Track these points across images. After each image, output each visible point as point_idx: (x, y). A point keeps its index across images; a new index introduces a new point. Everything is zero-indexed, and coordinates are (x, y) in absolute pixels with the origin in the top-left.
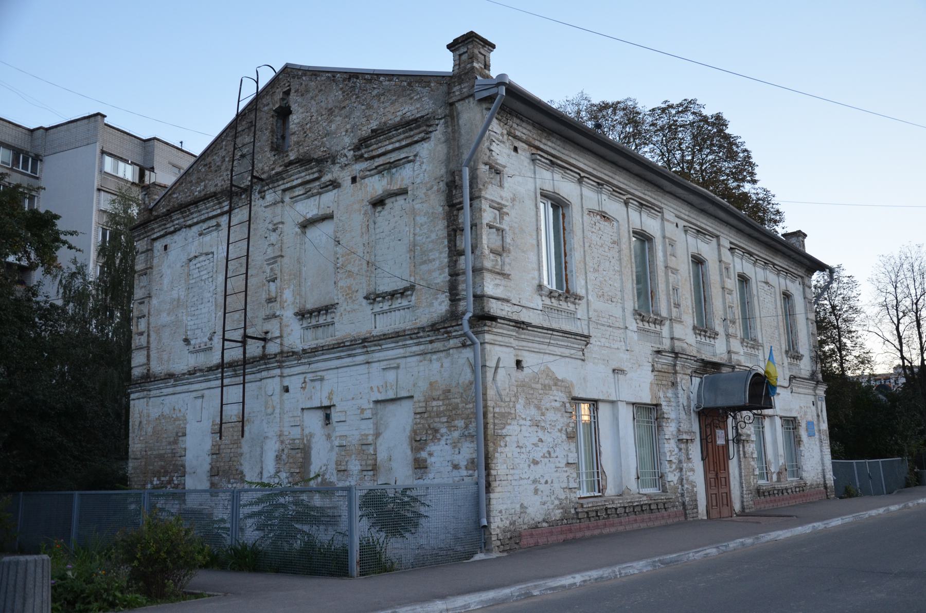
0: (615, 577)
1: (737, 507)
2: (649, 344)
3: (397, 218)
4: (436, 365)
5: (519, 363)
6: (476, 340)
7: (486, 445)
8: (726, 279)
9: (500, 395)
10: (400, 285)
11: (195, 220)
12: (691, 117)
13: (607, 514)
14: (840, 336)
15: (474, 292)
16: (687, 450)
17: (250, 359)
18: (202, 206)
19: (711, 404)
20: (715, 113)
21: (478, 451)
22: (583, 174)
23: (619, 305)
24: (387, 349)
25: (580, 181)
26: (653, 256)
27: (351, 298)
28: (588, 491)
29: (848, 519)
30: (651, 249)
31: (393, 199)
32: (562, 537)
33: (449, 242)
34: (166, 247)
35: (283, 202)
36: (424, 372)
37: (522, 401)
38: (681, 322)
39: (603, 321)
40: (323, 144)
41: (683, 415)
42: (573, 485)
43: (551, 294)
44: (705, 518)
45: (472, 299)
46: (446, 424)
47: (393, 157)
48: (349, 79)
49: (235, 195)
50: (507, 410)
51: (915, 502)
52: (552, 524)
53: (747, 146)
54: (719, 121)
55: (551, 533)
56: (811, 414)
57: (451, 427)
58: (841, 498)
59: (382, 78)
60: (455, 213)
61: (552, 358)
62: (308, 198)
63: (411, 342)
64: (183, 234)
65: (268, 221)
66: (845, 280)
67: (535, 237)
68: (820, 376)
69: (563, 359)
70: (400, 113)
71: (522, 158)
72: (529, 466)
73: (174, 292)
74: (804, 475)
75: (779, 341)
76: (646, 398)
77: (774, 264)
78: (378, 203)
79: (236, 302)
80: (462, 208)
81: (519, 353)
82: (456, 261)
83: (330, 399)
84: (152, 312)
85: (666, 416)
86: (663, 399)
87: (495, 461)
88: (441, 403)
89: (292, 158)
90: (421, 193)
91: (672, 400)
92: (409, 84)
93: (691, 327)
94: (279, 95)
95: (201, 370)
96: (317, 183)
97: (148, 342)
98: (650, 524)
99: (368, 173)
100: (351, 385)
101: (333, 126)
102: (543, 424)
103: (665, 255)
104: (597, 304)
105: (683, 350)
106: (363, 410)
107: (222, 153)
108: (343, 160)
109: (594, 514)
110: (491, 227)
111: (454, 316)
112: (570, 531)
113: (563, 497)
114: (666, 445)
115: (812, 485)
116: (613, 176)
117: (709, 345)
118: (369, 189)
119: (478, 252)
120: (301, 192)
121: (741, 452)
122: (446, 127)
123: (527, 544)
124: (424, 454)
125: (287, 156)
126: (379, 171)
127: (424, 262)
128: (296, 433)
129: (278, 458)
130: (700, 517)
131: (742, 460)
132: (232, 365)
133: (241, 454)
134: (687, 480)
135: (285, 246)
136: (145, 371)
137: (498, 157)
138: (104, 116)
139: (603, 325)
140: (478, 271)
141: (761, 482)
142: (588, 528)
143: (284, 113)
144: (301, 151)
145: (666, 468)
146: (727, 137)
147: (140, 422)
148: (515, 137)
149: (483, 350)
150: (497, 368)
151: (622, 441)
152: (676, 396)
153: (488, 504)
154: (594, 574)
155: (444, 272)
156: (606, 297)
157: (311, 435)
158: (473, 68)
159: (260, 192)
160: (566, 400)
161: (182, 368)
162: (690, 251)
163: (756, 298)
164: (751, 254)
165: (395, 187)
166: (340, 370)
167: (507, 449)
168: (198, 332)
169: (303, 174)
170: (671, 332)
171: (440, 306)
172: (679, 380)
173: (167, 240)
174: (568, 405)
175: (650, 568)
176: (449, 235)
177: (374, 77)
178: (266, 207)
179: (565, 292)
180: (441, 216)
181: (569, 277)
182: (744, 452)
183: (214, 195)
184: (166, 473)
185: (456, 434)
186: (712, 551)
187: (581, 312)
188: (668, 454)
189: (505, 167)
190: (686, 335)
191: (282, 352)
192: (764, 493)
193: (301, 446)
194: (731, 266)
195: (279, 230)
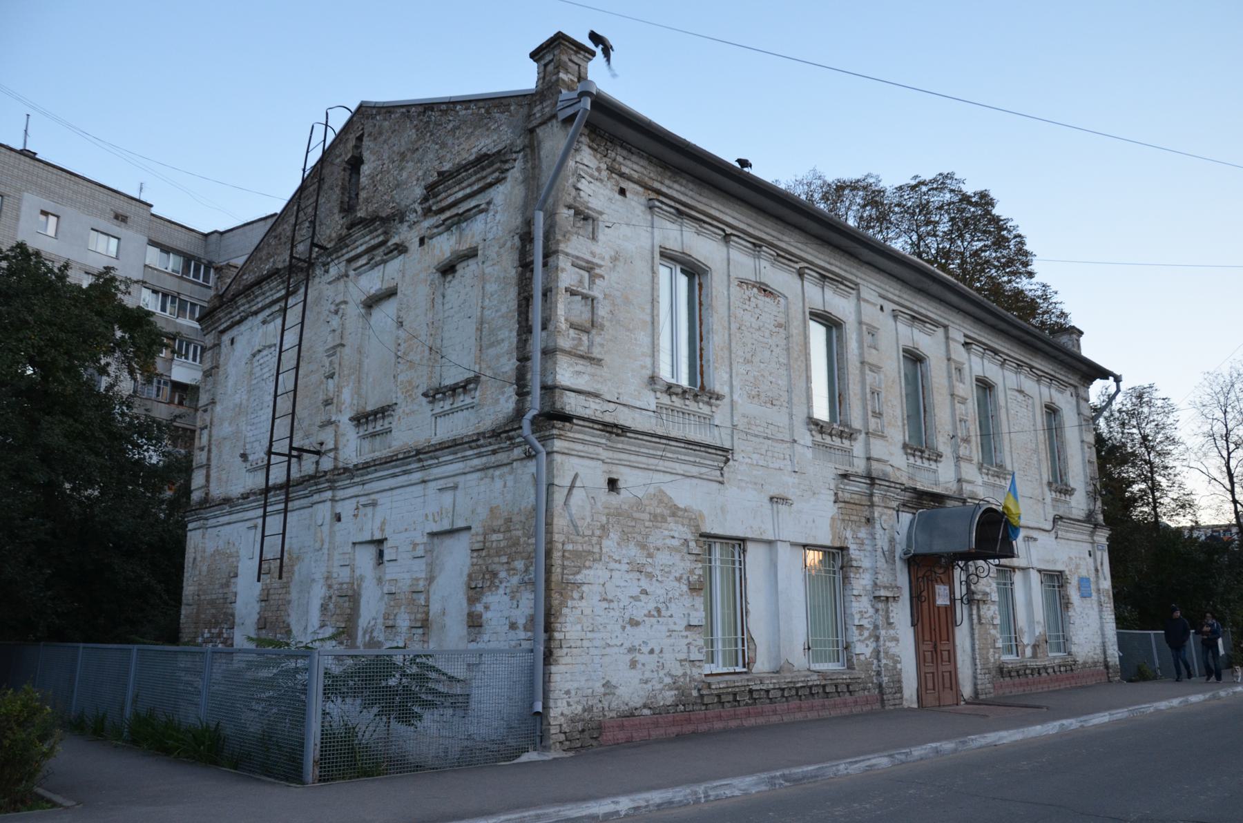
0: (697, 801)
1: (967, 691)
2: (831, 465)
4: (499, 484)
5: (613, 484)
7: (548, 597)
9: (575, 527)
10: (472, 375)
12: (948, 196)
13: (751, 697)
14: (1152, 472)
15: (542, 382)
16: (887, 611)
17: (300, 481)
19: (924, 550)
20: (979, 189)
22: (729, 231)
23: (784, 410)
25: (726, 238)
26: (842, 348)
28: (724, 665)
29: (1121, 714)
30: (840, 338)
31: (465, 264)
32: (674, 730)
35: (347, 276)
36: (485, 493)
37: (614, 536)
38: (883, 437)
39: (755, 430)
41: (882, 563)
42: (695, 656)
44: (915, 706)
46: (506, 566)
50: (586, 547)
51: (1230, 691)
52: (658, 712)
53: (1021, 231)
54: (985, 200)
55: (656, 725)
56: (1086, 568)
58: (1130, 681)
59: (458, 107)
61: (668, 477)
62: (372, 268)
63: (470, 452)
66: (1159, 403)
67: (649, 311)
68: (1101, 518)
69: (688, 480)
71: (633, 203)
72: (624, 628)
74: (1074, 649)
75: (1039, 469)
77: (1031, 367)
78: (448, 270)
81: (614, 468)
82: (526, 341)
83: (382, 530)
84: (215, 420)
85: (854, 564)
86: (851, 540)
87: (561, 620)
88: (501, 536)
91: (866, 542)
92: (488, 112)
93: (900, 445)
95: (254, 494)
97: (209, 459)
98: (825, 714)
100: (406, 509)
101: (405, 174)
102: (650, 570)
103: (861, 347)
105: (885, 474)
106: (415, 545)
108: (413, 217)
109: (730, 698)
110: (573, 293)
112: (689, 721)
113: (680, 672)
114: (854, 604)
115: (1085, 663)
116: (780, 236)
117: (928, 470)
118: (437, 252)
119: (551, 327)
121: (975, 617)
122: (526, 162)
123: (610, 741)
124: (479, 608)
127: (492, 345)
128: (344, 575)
129: (324, 608)
130: (906, 704)
133: (289, 602)
134: (886, 653)
137: (590, 199)
139: (756, 436)
140: (549, 353)
141: (1006, 658)
142: (720, 717)
143: (355, 164)
145: (854, 635)
146: (996, 220)
147: (195, 559)
148: (622, 175)
149: (550, 463)
150: (572, 487)
154: (656, 797)
156: (763, 398)
157: (362, 578)
158: (558, 79)
160: (689, 537)
162: (901, 343)
163: (1003, 411)
165: (464, 246)
166: (395, 492)
167: (583, 603)
169: (368, 238)
171: (506, 404)
172: (876, 515)
174: (692, 544)
175: (763, 788)
176: (520, 306)
178: (330, 283)
179: (700, 390)
181: (705, 368)
184: (217, 624)
185: (515, 580)
186: (882, 761)
187: (721, 415)
188: (857, 616)
189: (601, 213)
191: (336, 468)
192: (1009, 672)
193: (350, 593)
194: (966, 366)
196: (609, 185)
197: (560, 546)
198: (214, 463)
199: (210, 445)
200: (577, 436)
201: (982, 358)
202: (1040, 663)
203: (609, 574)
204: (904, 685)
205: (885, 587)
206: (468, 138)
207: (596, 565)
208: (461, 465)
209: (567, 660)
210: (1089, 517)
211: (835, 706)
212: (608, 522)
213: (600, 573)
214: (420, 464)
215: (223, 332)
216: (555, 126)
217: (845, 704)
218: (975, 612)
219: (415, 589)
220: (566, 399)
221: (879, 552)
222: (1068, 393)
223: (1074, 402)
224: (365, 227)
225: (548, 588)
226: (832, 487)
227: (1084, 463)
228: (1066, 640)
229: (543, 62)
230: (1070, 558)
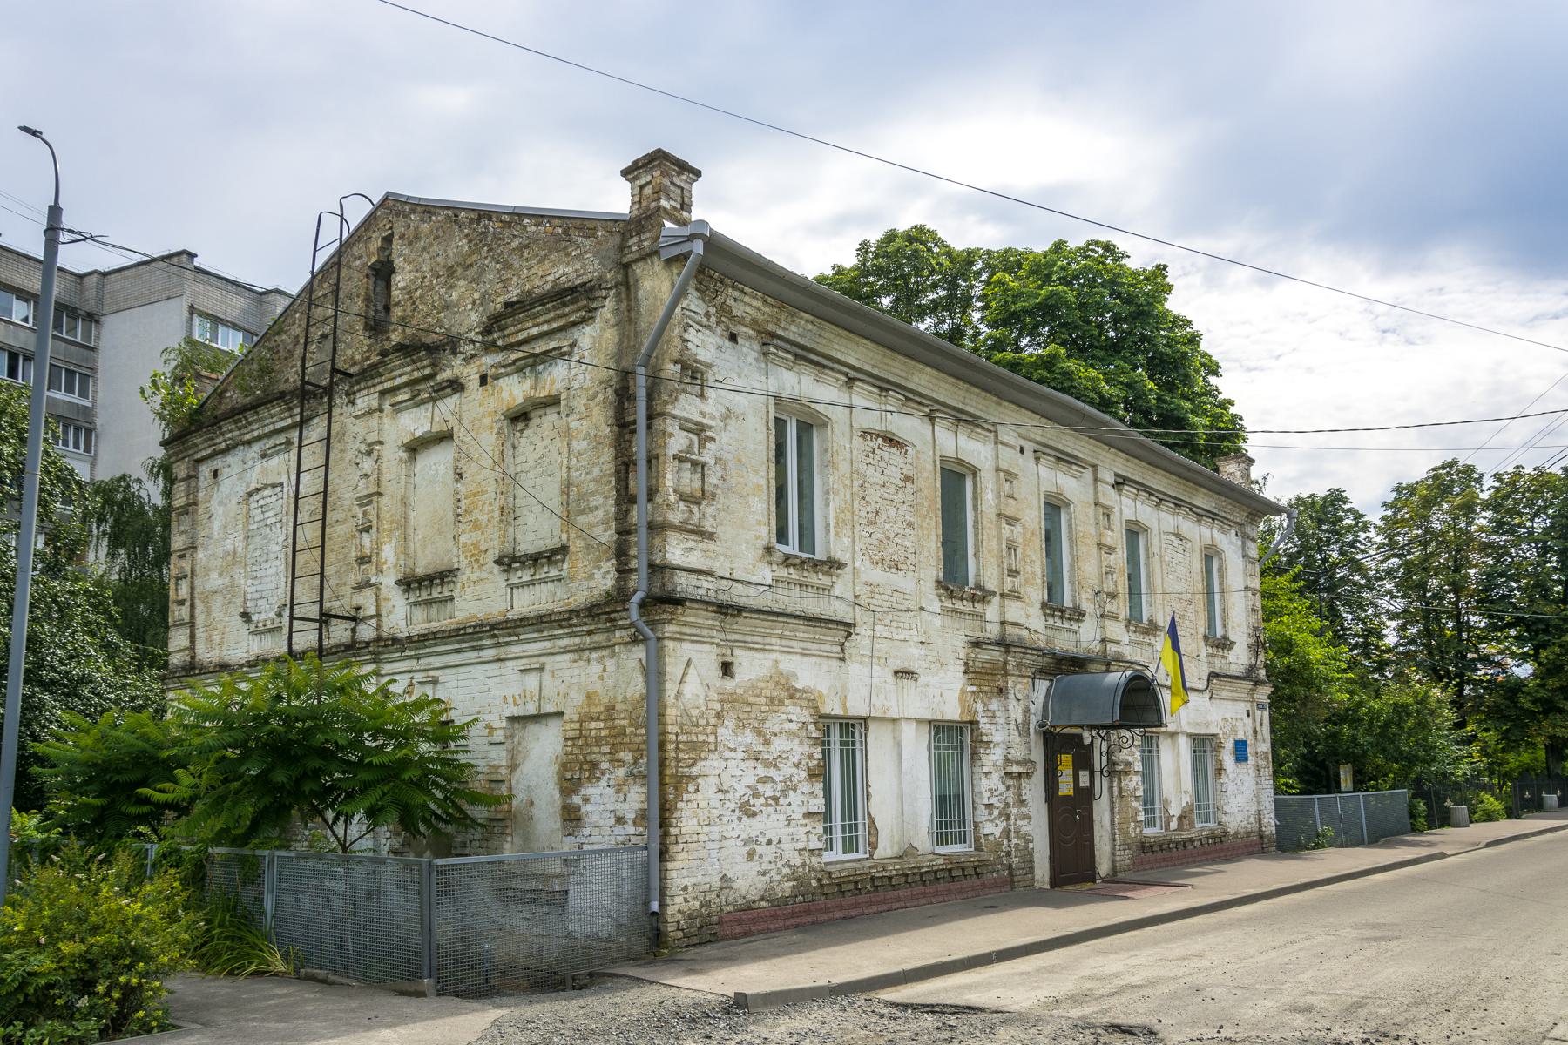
1: (1103, 867)
3: (547, 442)
4: (596, 668)
5: (727, 669)
6: (651, 634)
16: (1019, 788)
18: (264, 413)
24: (528, 641)
31: (541, 412)
33: (618, 480)
34: (215, 474)
35: (381, 410)
37: (730, 722)
38: (1019, 598)
40: (440, 323)
41: (1015, 737)
42: (815, 844)
43: (787, 561)
47: (540, 347)
48: (479, 219)
49: (311, 398)
50: (701, 738)
52: (776, 903)
55: (775, 917)
57: (616, 762)
59: (526, 221)
60: (627, 437)
65: (360, 439)
67: (763, 474)
68: (1263, 672)
70: (551, 278)
72: (740, 819)
76: (952, 712)
77: (1191, 507)
78: (520, 417)
79: (308, 561)
80: (634, 432)
82: (627, 512)
84: (198, 568)
87: (677, 814)
88: (602, 725)
90: (580, 403)
92: (566, 232)
94: (376, 244)
101: (455, 295)
105: (1021, 638)
108: (469, 348)
109: (851, 886)
111: (619, 597)
112: (808, 912)
113: (799, 862)
115: (1237, 833)
118: (505, 395)
119: (658, 500)
120: (406, 397)
121: (1115, 789)
122: (619, 302)
124: (577, 800)
125: (388, 339)
126: (519, 368)
127: (583, 512)
134: (1017, 832)
135: (384, 479)
137: (699, 351)
138: (192, 256)
141: (1147, 831)
142: (840, 907)
143: (383, 272)
156: (887, 563)
162: (1043, 489)
164: (1150, 492)
167: (699, 796)
169: (408, 369)
170: (1003, 613)
171: (603, 579)
172: (1010, 684)
173: (217, 463)
174: (812, 727)
176: (617, 472)
177: (515, 217)
178: (356, 417)
180: (607, 442)
182: (1120, 789)
183: (282, 395)
185: (621, 772)
189: (710, 366)
190: (1029, 618)
191: (379, 639)
194: (1116, 510)
196: (718, 330)
198: (199, 620)
199: (192, 598)
200: (691, 619)
203: (724, 764)
204: (1036, 865)
205: (1018, 763)
208: (547, 644)
210: (1249, 675)
213: (716, 764)
215: (199, 461)
216: (657, 265)
219: (494, 777)
220: (677, 579)
221: (1012, 726)
224: (406, 355)
225: (662, 783)
226: (962, 656)
230: (1225, 720)
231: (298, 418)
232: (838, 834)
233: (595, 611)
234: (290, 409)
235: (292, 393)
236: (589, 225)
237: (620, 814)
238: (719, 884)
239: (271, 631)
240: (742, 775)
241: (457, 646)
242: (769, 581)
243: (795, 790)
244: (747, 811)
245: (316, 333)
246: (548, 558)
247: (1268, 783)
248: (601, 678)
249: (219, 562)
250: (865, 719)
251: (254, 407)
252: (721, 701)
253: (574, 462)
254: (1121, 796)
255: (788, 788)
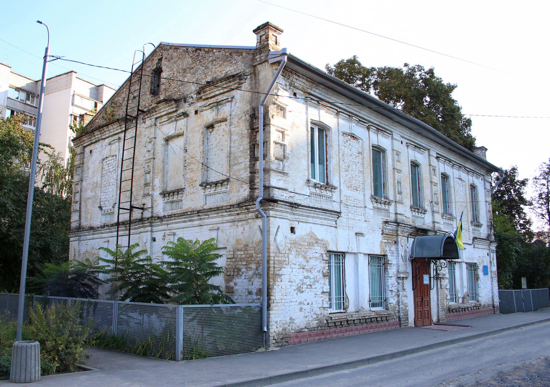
1: (435, 319)
2: (381, 217)
3: (221, 136)
4: (240, 229)
5: (292, 230)
7: (268, 281)
8: (433, 177)
10: (224, 178)
11: (107, 136)
16: (403, 284)
18: (110, 127)
21: (263, 284)
22: (339, 110)
24: (212, 218)
26: (385, 162)
27: (192, 185)
28: (336, 309)
31: (219, 124)
35: (156, 125)
37: (294, 253)
41: (401, 262)
43: (315, 186)
45: (262, 188)
47: (220, 98)
52: (311, 330)
55: (310, 335)
57: (248, 268)
60: (254, 134)
62: (170, 123)
63: (226, 214)
64: (101, 144)
65: (146, 137)
67: (306, 149)
68: (493, 237)
72: (297, 294)
73: (95, 178)
74: (480, 299)
77: (465, 167)
78: (210, 126)
79: (126, 185)
81: (293, 223)
82: (254, 164)
84: (83, 189)
85: (390, 262)
86: (388, 252)
87: (274, 291)
88: (242, 253)
89: (161, 99)
91: (395, 252)
92: (231, 54)
94: (156, 61)
95: (108, 226)
96: (175, 114)
97: (80, 208)
99: (204, 108)
104: (346, 192)
105: (403, 220)
107: (123, 95)
108: (191, 100)
109: (339, 324)
111: (252, 199)
112: (323, 334)
114: (389, 281)
115: (484, 305)
116: (360, 111)
118: (205, 118)
119: (267, 159)
120: (166, 120)
121: (439, 285)
122: (251, 80)
124: (232, 284)
127: (235, 164)
130: (409, 325)
131: (439, 290)
132: (123, 223)
134: (402, 302)
135: (156, 152)
136: (78, 225)
140: (267, 171)
142: (335, 332)
143: (158, 71)
144: (167, 95)
145: (389, 295)
147: (75, 255)
151: (360, 278)
152: (397, 250)
153: (268, 317)
155: (247, 171)
159: (143, 119)
160: (323, 252)
161: (98, 223)
163: (452, 189)
164: (450, 161)
165: (220, 117)
168: (107, 202)
169: (167, 109)
171: (244, 192)
173: (92, 147)
174: (324, 256)
176: (250, 148)
177: (210, 49)
180: (246, 136)
181: (328, 174)
182: (441, 285)
183: (118, 120)
185: (251, 273)
187: (336, 196)
188: (390, 286)
189: (287, 105)
191: (152, 217)
192: (453, 310)
194: (437, 168)
195: (153, 142)
197: (273, 258)
200: (279, 209)
201: (444, 164)
202: (465, 306)
204: (409, 317)
205: (403, 273)
206: (220, 66)
207: (287, 266)
208: (220, 219)
209: (276, 308)
210: (488, 238)
211: (381, 326)
212: (291, 247)
214: (199, 217)
215: (85, 147)
217: (385, 326)
218: (439, 283)
220: (274, 192)
221: (400, 257)
222: (480, 179)
223: (483, 183)
225: (268, 277)
227: (486, 212)
228: (477, 294)
229: (260, 35)
231: (124, 129)
232: (334, 301)
233: (241, 205)
234: (120, 126)
235: (122, 119)
236: (240, 51)
237: (250, 290)
238: (289, 321)
239: (110, 214)
240: (297, 275)
241: (183, 220)
242: (308, 194)
243: (318, 282)
244: (300, 290)
245: (131, 96)
246: (221, 183)
247: (496, 284)
248: (242, 233)
249: (91, 187)
250: (344, 253)
251: (107, 125)
252: (291, 244)
253: (232, 144)
254: (441, 288)
255: (315, 281)
